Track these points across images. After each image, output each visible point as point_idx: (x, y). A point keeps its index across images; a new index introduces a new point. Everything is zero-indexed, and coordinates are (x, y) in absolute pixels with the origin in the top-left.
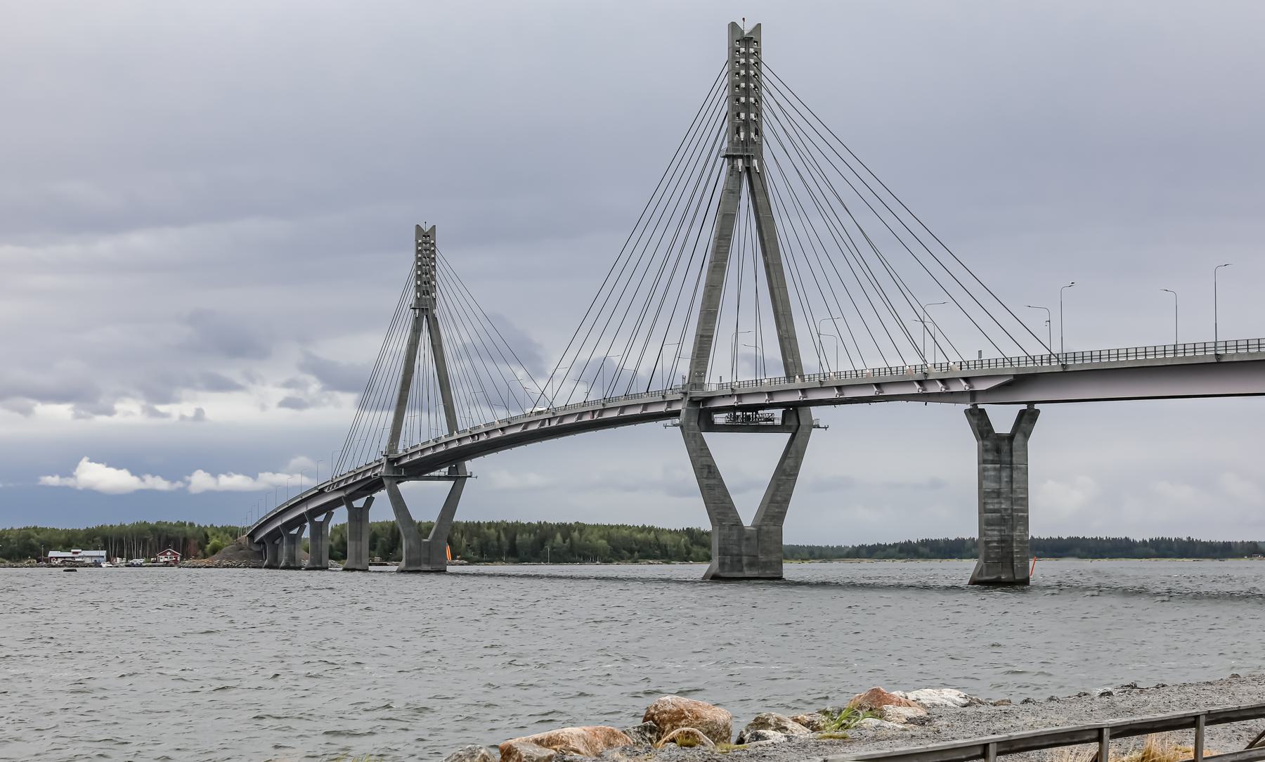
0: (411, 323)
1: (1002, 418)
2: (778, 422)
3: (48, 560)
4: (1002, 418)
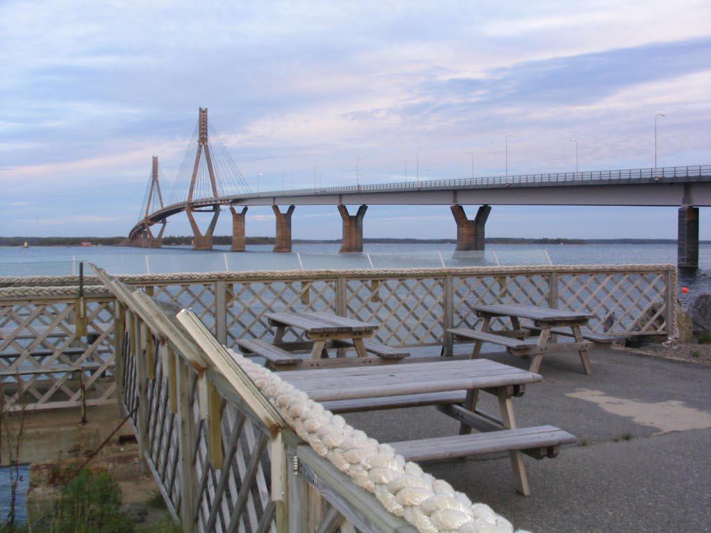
1: (353, 210)
4: (471, 212)
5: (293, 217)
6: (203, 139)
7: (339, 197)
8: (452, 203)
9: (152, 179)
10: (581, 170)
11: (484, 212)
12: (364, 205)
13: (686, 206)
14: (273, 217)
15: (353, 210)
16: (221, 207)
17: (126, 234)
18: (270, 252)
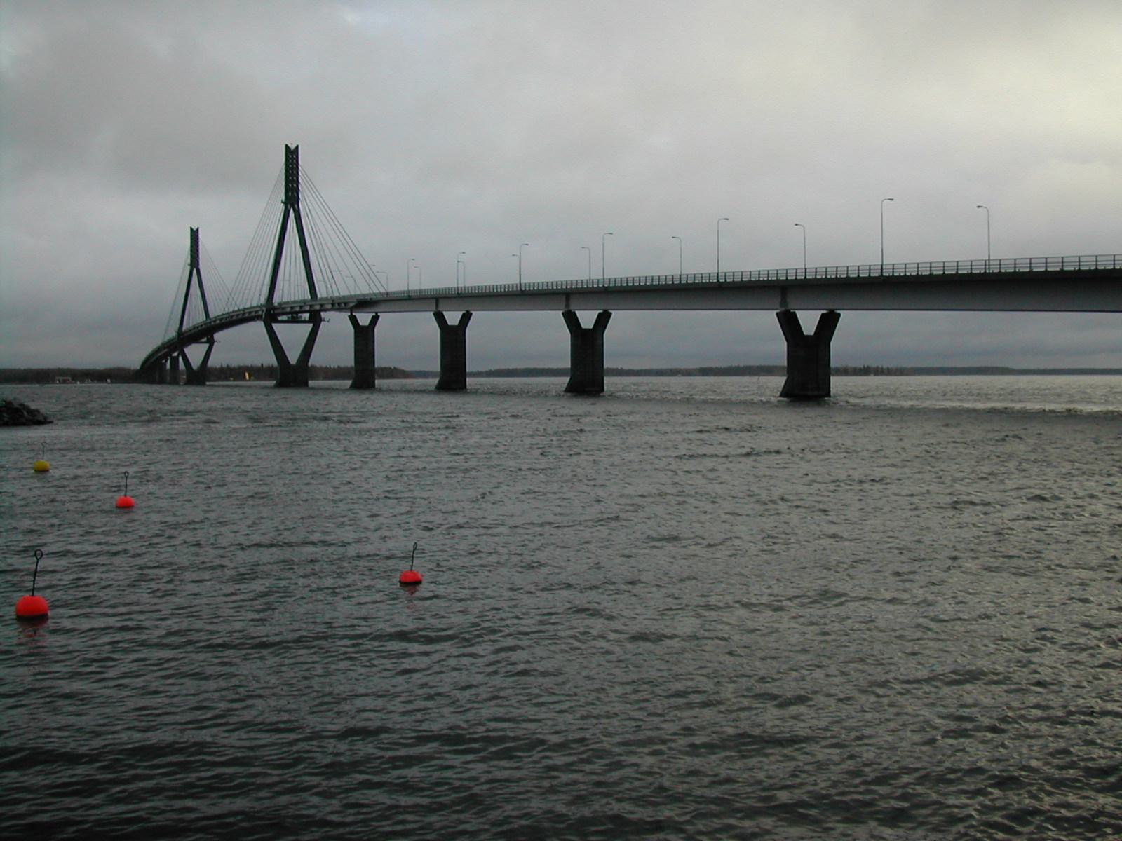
1: (587, 319)
2: (307, 319)
4: (809, 321)
5: (469, 331)
6: (292, 198)
7: (436, 301)
8: (778, 307)
9: (188, 268)
10: (995, 256)
11: (828, 323)
12: (468, 312)
13: (783, 309)
14: (566, 334)
15: (587, 319)
16: (323, 314)
17: (134, 361)
18: (429, 392)
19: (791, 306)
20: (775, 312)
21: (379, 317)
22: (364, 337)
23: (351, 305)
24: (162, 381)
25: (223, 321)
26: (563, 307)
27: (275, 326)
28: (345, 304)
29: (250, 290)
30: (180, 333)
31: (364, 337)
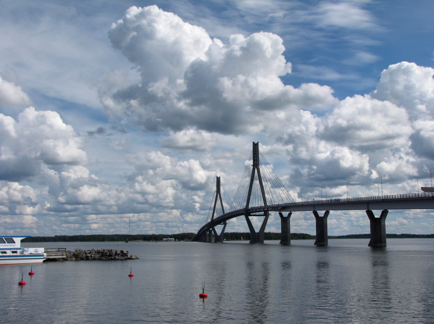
0: (248, 193)
1: (377, 214)
2: (263, 214)
3: (163, 240)
4: (377, 214)
16: (270, 212)
19: (316, 210)
20: (365, 210)
21: (292, 213)
22: (285, 222)
23: (279, 208)
24: (205, 241)
25: (229, 215)
26: (313, 210)
27: (250, 217)
28: (277, 208)
29: (258, 200)
30: (212, 220)
31: (285, 222)
